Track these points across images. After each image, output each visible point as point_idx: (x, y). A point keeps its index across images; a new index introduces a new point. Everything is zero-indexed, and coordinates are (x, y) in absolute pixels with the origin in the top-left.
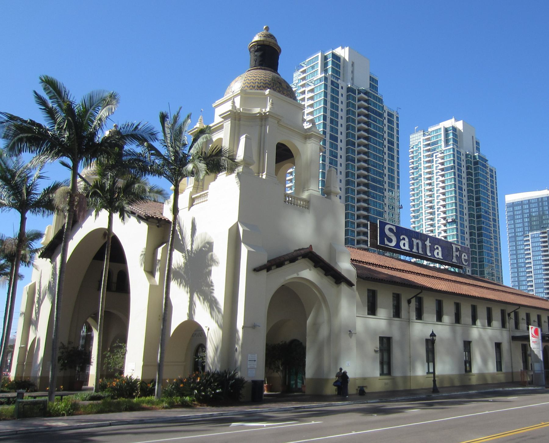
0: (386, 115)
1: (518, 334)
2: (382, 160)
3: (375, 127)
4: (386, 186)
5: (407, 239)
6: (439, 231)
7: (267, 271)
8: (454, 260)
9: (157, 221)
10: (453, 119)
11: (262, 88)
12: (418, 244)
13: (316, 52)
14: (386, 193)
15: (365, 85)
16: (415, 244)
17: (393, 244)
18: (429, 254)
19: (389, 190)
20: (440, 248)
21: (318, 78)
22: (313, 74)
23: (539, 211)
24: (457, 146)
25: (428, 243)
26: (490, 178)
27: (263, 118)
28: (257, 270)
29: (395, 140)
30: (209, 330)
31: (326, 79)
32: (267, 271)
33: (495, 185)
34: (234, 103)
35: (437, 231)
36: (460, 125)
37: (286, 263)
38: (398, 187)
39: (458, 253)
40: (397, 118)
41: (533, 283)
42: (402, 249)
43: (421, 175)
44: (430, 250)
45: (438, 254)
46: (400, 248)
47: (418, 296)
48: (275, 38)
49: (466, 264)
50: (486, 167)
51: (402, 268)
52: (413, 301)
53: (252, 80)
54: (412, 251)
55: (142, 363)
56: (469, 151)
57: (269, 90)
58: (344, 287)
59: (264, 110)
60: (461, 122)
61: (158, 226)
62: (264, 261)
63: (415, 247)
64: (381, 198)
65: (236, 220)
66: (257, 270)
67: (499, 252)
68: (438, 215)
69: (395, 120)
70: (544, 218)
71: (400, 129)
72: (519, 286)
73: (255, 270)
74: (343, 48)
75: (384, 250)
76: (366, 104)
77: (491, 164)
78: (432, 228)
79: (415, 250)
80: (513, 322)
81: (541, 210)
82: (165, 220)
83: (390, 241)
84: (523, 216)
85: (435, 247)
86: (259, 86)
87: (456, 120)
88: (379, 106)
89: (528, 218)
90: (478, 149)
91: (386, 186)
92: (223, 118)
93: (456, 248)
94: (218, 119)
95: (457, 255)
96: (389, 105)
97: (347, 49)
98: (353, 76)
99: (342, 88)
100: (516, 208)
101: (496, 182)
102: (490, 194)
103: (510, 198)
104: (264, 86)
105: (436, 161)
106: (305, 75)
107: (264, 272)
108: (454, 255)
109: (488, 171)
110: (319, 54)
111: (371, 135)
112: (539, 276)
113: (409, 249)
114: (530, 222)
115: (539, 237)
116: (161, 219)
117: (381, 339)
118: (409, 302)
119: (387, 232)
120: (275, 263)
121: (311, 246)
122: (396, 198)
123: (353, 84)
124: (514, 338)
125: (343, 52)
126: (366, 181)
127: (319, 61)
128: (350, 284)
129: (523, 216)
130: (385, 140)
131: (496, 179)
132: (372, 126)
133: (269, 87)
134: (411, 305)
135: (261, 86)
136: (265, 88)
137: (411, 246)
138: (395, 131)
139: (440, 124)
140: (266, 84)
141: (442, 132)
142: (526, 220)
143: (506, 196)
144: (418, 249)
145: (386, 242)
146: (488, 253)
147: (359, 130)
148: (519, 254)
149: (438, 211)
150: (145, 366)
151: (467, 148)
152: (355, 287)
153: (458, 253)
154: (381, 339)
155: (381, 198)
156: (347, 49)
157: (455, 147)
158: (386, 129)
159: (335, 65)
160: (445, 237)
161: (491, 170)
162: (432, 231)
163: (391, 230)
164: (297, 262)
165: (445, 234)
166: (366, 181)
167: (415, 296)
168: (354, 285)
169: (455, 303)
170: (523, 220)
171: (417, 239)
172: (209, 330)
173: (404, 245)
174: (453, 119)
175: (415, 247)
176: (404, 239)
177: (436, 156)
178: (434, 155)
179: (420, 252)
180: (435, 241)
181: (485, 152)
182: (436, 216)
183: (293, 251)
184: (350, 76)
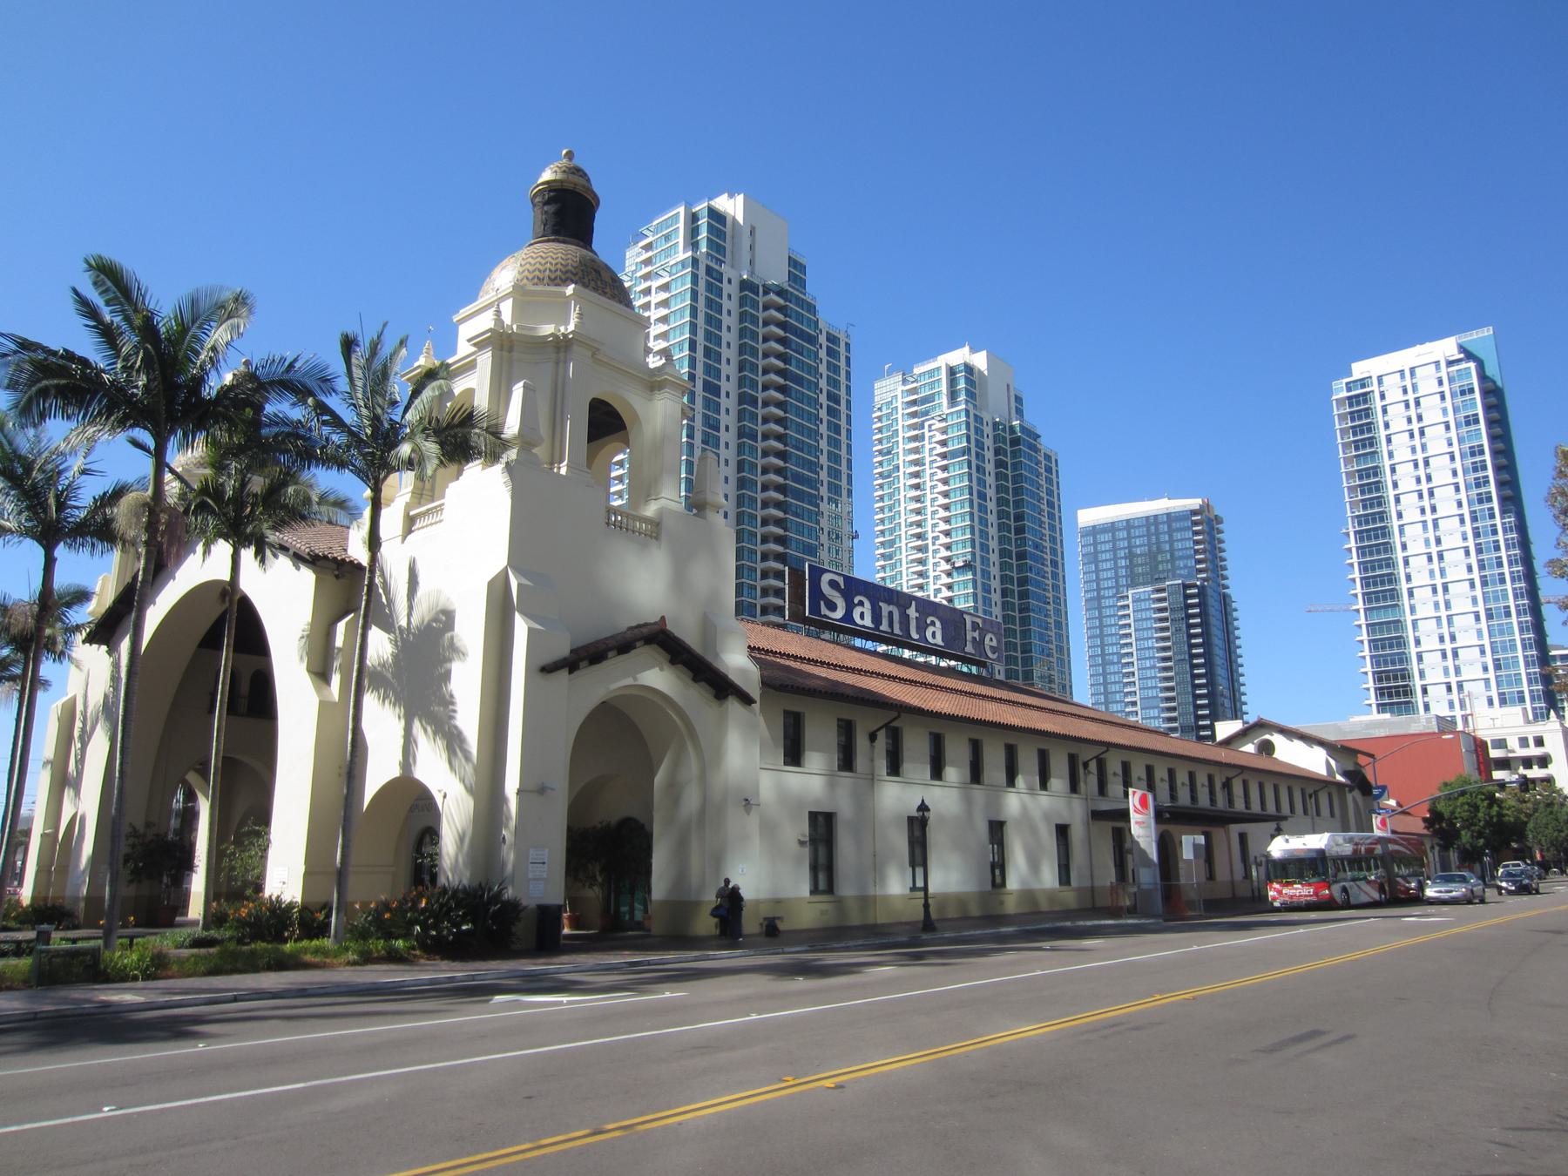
0: (822, 339)
1: (1104, 806)
2: (815, 434)
4: (824, 491)
5: (867, 604)
8: (969, 648)
10: (967, 349)
12: (891, 613)
15: (777, 275)
16: (885, 613)
19: (830, 499)
20: (938, 624)
22: (668, 252)
23: (1149, 545)
25: (912, 612)
27: (561, 346)
28: (548, 669)
31: (695, 262)
34: (498, 313)
35: (932, 588)
37: (610, 654)
38: (850, 492)
39: (976, 634)
40: (847, 345)
43: (897, 468)
44: (918, 628)
45: (935, 634)
50: (1037, 450)
51: (858, 666)
52: (882, 735)
55: (302, 869)
58: (733, 705)
59: (562, 329)
62: (562, 649)
63: (885, 622)
66: (548, 669)
69: (842, 349)
72: (1107, 703)
73: (544, 669)
74: (731, 196)
77: (1046, 443)
78: (920, 581)
79: (884, 627)
80: (1093, 780)
83: (832, 607)
87: (974, 350)
90: (1019, 412)
91: (824, 491)
94: (464, 349)
96: (830, 317)
97: (740, 198)
98: (753, 256)
99: (730, 281)
100: (1101, 538)
103: (1089, 516)
106: (650, 254)
107: (564, 673)
108: (969, 638)
110: (681, 210)
111: (791, 382)
114: (1131, 567)
117: (813, 816)
118: (873, 737)
119: (826, 589)
121: (663, 618)
122: (844, 515)
123: (752, 273)
124: (1097, 815)
125: (732, 206)
126: (780, 480)
128: (746, 700)
136: (565, 282)
137: (877, 618)
144: (891, 625)
145: (824, 611)
151: (996, 408)
152: (756, 706)
153: (976, 634)
154: (813, 816)
156: (740, 198)
157: (971, 407)
160: (950, 600)
162: (921, 587)
163: (833, 584)
165: (950, 594)
167: (886, 726)
173: (862, 616)
174: (967, 349)
175: (885, 622)
179: (897, 631)
180: (927, 607)
181: (1035, 417)
184: (746, 256)
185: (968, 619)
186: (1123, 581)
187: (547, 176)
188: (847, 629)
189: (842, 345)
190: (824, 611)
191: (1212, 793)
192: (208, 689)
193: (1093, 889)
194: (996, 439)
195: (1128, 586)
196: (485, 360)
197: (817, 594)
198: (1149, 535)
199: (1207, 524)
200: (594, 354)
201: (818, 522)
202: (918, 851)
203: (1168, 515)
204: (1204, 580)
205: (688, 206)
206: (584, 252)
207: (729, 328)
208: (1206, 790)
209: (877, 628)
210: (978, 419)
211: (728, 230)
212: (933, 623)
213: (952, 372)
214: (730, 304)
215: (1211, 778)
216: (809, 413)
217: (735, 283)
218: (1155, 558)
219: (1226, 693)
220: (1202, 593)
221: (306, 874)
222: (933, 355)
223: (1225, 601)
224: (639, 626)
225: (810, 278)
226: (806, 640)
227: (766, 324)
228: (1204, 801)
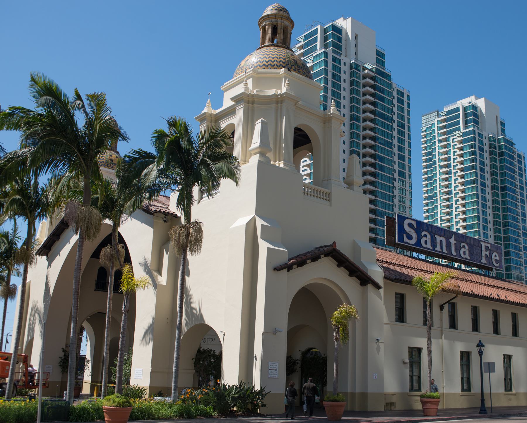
0: (395, 94)
4: (396, 175)
5: (429, 236)
7: (288, 271)
8: (484, 261)
9: (164, 216)
10: (473, 97)
11: (275, 67)
12: (441, 241)
13: (316, 25)
14: (396, 184)
16: (438, 241)
17: (413, 241)
18: (454, 253)
19: (399, 180)
21: (317, 53)
24: (478, 128)
25: (452, 241)
27: (278, 100)
28: (277, 269)
29: (406, 122)
30: (224, 335)
31: (326, 54)
32: (288, 271)
33: (523, 173)
34: (246, 84)
36: (481, 103)
37: (309, 261)
38: (410, 176)
39: (487, 253)
40: (408, 96)
42: (423, 247)
43: (435, 163)
44: (456, 249)
45: (465, 253)
46: (421, 245)
47: (452, 301)
48: (287, 10)
50: (513, 152)
51: (428, 269)
52: (446, 307)
53: (265, 59)
54: (435, 250)
55: (150, 369)
56: (492, 134)
57: (283, 69)
59: (279, 92)
61: (165, 221)
63: (438, 246)
64: (391, 189)
66: (277, 269)
68: (457, 208)
71: (411, 110)
73: (276, 268)
74: (345, 19)
76: (372, 82)
77: (519, 148)
79: (438, 248)
82: (172, 214)
83: (410, 237)
85: (461, 246)
86: (273, 64)
87: (477, 98)
88: (388, 83)
90: (503, 131)
92: (234, 101)
93: (486, 246)
95: (486, 255)
96: (399, 81)
97: (350, 20)
99: (345, 64)
102: (518, 183)
105: (454, 146)
108: (483, 255)
110: (319, 27)
113: (431, 248)
116: (168, 213)
118: (442, 307)
119: (407, 228)
120: (300, 261)
121: (334, 242)
123: (356, 59)
125: (345, 24)
126: (373, 170)
127: (318, 35)
130: (394, 122)
131: (525, 166)
132: (379, 106)
133: (284, 65)
134: (444, 311)
135: (274, 65)
136: (279, 67)
138: (406, 112)
139: (458, 102)
141: (461, 112)
145: (406, 239)
149: (456, 204)
150: (153, 374)
151: (490, 130)
152: (382, 291)
153: (487, 253)
155: (391, 189)
156: (350, 20)
157: (476, 129)
158: (395, 109)
161: (519, 156)
163: (410, 225)
166: (373, 170)
169: (493, 310)
171: (440, 236)
172: (224, 335)
173: (426, 242)
174: (473, 97)
175: (438, 246)
176: (425, 236)
178: (451, 139)
179: (454, 253)
181: (510, 134)
182: (454, 209)
183: (313, 249)
184: (353, 50)
185: (483, 244)
187: (269, 11)
188: (418, 248)
189: (405, 96)
190: (406, 239)
193: (489, 372)
196: (240, 111)
197: (402, 230)
200: (296, 104)
202: (465, 368)
205: (322, 25)
206: (288, 51)
207: (345, 89)
209: (434, 249)
210: (480, 135)
211: (343, 37)
213: (465, 109)
214: (345, 76)
216: (388, 133)
217: (348, 65)
224: (321, 247)
227: (364, 86)
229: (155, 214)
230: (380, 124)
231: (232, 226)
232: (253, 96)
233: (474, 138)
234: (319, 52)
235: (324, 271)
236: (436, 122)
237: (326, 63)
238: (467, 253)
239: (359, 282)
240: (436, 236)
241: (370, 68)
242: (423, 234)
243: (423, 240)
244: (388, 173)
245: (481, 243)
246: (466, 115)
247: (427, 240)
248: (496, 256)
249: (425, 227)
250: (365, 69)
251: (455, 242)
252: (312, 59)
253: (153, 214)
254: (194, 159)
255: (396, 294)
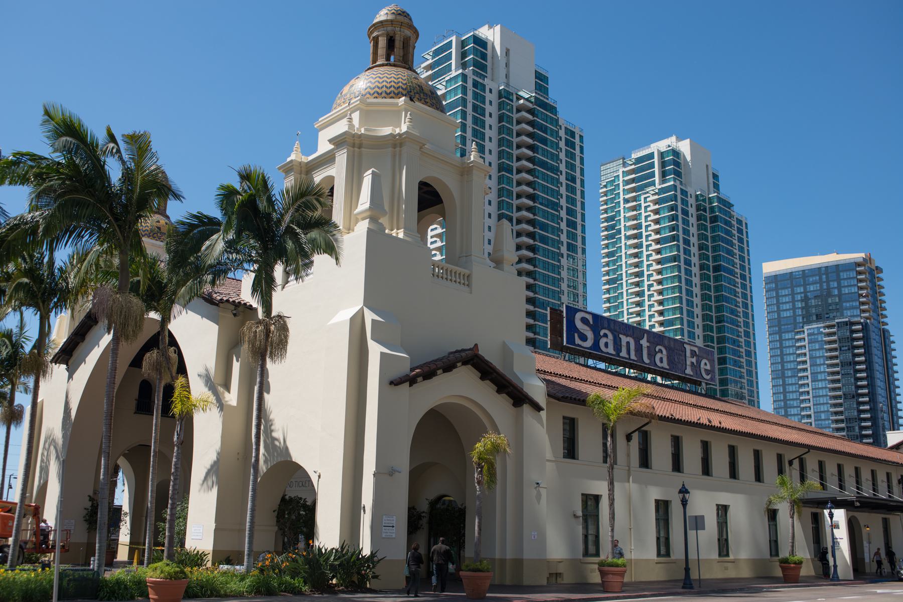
0: (562, 133)
3: (545, 153)
4: (564, 249)
5: (610, 336)
6: (652, 323)
7: (411, 385)
8: (689, 371)
9: (233, 307)
10: (674, 138)
11: (392, 95)
12: (628, 343)
16: (624, 343)
17: (589, 343)
19: (568, 256)
20: (664, 352)
21: (452, 76)
24: (681, 182)
25: (644, 342)
26: (737, 234)
27: (396, 142)
28: (395, 383)
30: (319, 477)
32: (411, 385)
36: (685, 147)
37: (439, 372)
38: (584, 251)
39: (694, 360)
40: (581, 137)
41: (811, 412)
42: (602, 352)
43: (619, 232)
44: (649, 354)
45: (662, 360)
46: (600, 350)
47: (644, 428)
49: (708, 377)
50: (731, 217)
51: (609, 384)
52: (636, 437)
54: (619, 356)
55: (213, 526)
56: (701, 190)
57: (404, 98)
59: (398, 131)
60: (687, 141)
61: (235, 315)
62: (404, 369)
63: (624, 349)
65: (359, 305)
66: (395, 383)
67: (753, 359)
69: (577, 141)
70: (830, 301)
73: (394, 382)
74: (490, 27)
75: (575, 353)
77: (738, 210)
79: (624, 353)
80: (796, 474)
81: (825, 287)
82: (245, 304)
83: (584, 338)
84: (793, 298)
86: (388, 91)
87: (680, 139)
88: (552, 118)
89: (802, 301)
90: (716, 187)
95: (692, 363)
96: (567, 116)
97: (498, 28)
99: (491, 91)
101: (748, 242)
102: (737, 261)
103: (771, 267)
104: (396, 92)
108: (688, 363)
109: (734, 223)
110: (454, 38)
111: (542, 166)
112: (822, 400)
113: (614, 353)
114: (806, 308)
115: (822, 333)
116: (239, 303)
118: (629, 438)
119: (579, 325)
121: (476, 345)
123: (507, 85)
125: (492, 34)
126: (531, 242)
127: (453, 50)
129: (793, 298)
132: (540, 151)
133: (404, 93)
136: (398, 95)
139: (652, 145)
140: (398, 88)
142: (799, 305)
143: (764, 265)
144: (629, 352)
145: (578, 341)
146: (735, 361)
147: (519, 159)
148: (787, 362)
149: (649, 290)
151: (697, 185)
152: (543, 414)
153: (694, 360)
156: (498, 28)
157: (678, 183)
158: (562, 156)
159: (479, 54)
161: (739, 222)
163: (584, 321)
164: (454, 370)
166: (531, 242)
168: (542, 409)
169: (702, 441)
170: (794, 305)
171: (627, 336)
172: (319, 477)
174: (674, 138)
175: (624, 349)
177: (645, 198)
178: (642, 197)
179: (633, 357)
181: (727, 191)
182: (646, 298)
184: (502, 71)
185: (688, 348)
186: (800, 319)
188: (595, 353)
190: (578, 341)
191: (889, 487)
192: (145, 394)
194: (698, 208)
195: (804, 323)
196: (342, 158)
198: (820, 282)
199: (869, 274)
201: (559, 274)
202: (662, 523)
203: (837, 266)
204: (867, 318)
205: (459, 35)
208: (885, 485)
210: (684, 193)
212: (606, 335)
214: (491, 109)
215: (888, 475)
217: (495, 92)
218: (827, 300)
219: (885, 408)
220: (865, 328)
221: (217, 531)
222: (648, 144)
223: (885, 335)
224: (457, 351)
225: (551, 87)
226: (566, 364)
228: (883, 495)
229: (221, 305)
230: (540, 176)
231: (333, 321)
232: (360, 136)
233: (676, 196)
234: (454, 73)
235: (461, 387)
236: (620, 173)
237: (464, 89)
238: (665, 360)
239: (512, 401)
240: (621, 336)
241: (527, 96)
242: (602, 333)
243: (603, 341)
244: (553, 246)
245: (685, 346)
246: (663, 164)
247: (608, 341)
248: (706, 364)
249: (606, 322)
250: (519, 98)
251: (648, 344)
252: (444, 83)
253: (217, 305)
254: (276, 227)
255: (564, 418)
